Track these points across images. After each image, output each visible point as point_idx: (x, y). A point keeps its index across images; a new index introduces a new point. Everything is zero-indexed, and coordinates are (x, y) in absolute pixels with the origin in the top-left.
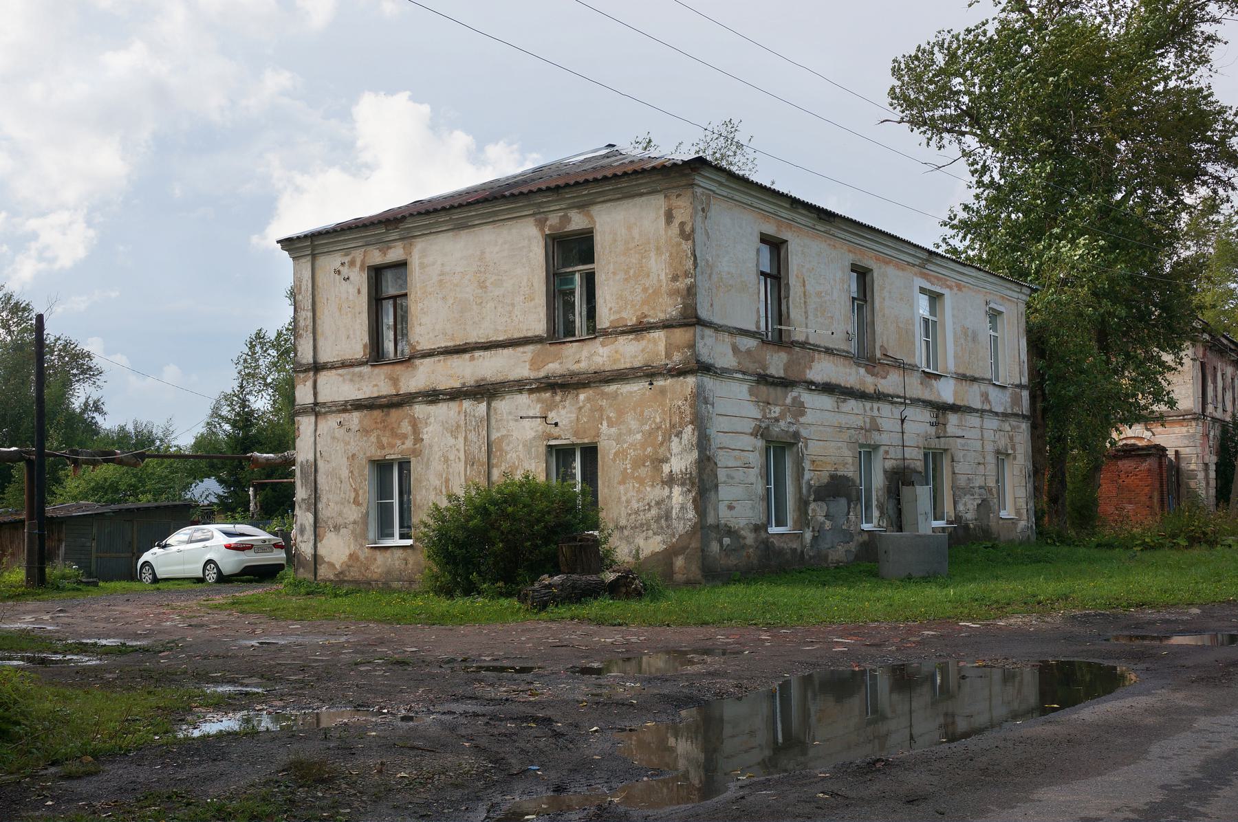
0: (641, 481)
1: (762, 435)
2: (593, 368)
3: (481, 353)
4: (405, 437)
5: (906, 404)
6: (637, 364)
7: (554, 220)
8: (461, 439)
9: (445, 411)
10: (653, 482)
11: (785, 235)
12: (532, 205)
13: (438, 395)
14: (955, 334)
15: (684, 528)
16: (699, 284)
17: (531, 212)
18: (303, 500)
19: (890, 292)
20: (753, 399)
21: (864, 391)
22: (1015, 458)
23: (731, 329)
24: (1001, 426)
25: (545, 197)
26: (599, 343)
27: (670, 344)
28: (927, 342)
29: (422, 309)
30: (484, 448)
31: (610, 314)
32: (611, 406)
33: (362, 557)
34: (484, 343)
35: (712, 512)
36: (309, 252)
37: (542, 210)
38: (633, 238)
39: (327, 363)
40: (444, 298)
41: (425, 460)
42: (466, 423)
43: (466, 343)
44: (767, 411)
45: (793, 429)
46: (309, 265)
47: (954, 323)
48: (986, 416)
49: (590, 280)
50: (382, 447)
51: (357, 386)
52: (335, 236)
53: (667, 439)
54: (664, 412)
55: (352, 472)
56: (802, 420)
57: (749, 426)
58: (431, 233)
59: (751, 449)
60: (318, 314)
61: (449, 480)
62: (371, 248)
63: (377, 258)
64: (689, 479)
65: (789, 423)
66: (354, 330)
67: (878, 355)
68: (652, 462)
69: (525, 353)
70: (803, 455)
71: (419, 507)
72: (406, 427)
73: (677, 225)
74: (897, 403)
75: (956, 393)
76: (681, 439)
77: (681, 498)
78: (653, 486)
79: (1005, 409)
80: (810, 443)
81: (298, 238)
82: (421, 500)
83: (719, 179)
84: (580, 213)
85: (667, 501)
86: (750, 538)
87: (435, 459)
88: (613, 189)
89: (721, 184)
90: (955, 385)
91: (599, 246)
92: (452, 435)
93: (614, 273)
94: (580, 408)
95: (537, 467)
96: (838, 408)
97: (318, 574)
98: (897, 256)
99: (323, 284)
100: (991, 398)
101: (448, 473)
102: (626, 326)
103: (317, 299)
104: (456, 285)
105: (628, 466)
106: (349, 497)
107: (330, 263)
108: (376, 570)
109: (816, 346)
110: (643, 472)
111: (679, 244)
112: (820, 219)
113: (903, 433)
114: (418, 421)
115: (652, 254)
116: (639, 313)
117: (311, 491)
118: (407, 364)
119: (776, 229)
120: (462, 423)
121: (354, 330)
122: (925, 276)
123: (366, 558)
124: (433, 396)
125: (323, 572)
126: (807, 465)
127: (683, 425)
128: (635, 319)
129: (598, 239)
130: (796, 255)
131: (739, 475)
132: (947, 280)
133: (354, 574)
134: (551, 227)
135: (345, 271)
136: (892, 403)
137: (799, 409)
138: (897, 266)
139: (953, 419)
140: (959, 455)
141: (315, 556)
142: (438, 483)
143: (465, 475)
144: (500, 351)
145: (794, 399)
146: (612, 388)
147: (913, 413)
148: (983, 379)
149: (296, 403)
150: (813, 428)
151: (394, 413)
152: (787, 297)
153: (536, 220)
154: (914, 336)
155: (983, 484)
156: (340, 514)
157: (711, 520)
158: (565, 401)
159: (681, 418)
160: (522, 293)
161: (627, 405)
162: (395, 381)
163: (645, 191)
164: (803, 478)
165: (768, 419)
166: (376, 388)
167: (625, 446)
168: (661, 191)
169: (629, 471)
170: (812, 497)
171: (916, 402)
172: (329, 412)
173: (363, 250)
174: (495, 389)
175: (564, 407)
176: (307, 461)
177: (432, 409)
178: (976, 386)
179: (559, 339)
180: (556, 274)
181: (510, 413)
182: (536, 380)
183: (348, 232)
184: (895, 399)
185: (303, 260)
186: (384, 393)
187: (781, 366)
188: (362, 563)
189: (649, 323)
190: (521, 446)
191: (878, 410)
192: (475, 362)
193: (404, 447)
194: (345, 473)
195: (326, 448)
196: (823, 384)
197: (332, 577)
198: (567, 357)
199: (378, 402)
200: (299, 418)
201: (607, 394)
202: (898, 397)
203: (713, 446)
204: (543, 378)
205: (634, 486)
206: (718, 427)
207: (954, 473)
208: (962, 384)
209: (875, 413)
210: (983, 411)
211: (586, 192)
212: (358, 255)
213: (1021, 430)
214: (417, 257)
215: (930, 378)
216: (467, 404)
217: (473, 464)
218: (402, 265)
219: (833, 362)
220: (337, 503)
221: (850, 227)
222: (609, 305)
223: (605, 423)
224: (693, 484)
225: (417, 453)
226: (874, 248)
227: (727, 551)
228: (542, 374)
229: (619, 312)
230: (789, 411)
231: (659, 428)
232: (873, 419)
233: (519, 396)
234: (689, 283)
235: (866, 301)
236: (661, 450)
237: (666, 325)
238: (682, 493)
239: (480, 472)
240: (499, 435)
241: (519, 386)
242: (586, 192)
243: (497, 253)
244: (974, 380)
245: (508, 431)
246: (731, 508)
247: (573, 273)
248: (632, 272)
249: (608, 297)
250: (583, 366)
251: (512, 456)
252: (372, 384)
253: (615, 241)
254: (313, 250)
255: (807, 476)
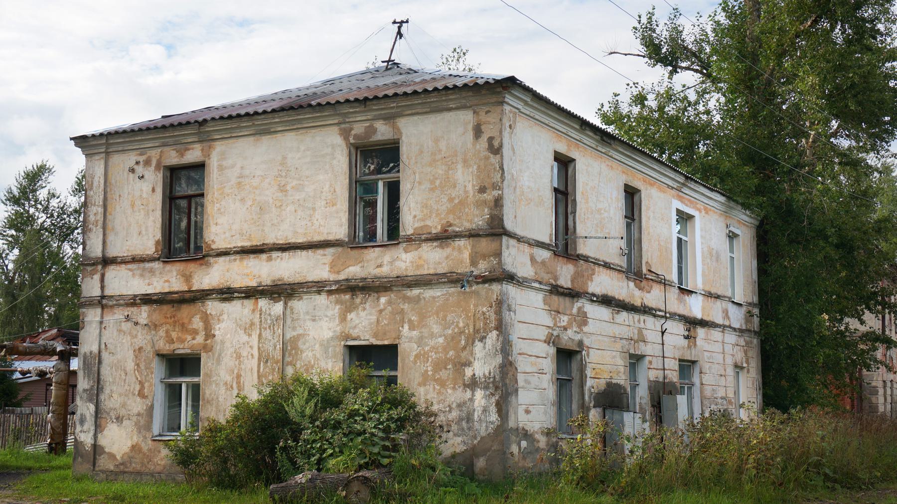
0: (442, 384)
1: (553, 343)
2: (395, 273)
3: (279, 254)
4: (195, 332)
5: (666, 318)
6: (440, 270)
7: (359, 129)
8: (255, 337)
9: (239, 310)
10: (454, 385)
11: (573, 154)
12: (338, 114)
13: (233, 293)
14: (703, 253)
15: (486, 430)
16: (505, 196)
17: (336, 121)
18: (85, 391)
19: (654, 212)
20: (547, 307)
21: (633, 305)
22: (748, 372)
23: (531, 241)
24: (738, 341)
25: (351, 107)
26: (402, 248)
27: (476, 253)
28: (732, 258)
29: (219, 209)
30: (279, 346)
31: (414, 222)
32: (413, 310)
33: (145, 448)
34: (282, 244)
35: (513, 415)
36: (103, 150)
37: (347, 120)
38: (440, 151)
39: (118, 257)
40: (243, 200)
41: (216, 355)
42: (261, 321)
43: (263, 244)
44: (558, 320)
45: (577, 337)
46: (102, 162)
47: (702, 243)
48: (726, 331)
49: (394, 191)
50: (172, 341)
51: (147, 281)
52: (132, 136)
53: (471, 342)
54: (468, 317)
55: (138, 365)
56: (585, 329)
57: (542, 334)
58: (231, 137)
59: (544, 356)
60: (109, 209)
61: (241, 375)
62: (166, 149)
63: (173, 158)
64: (493, 382)
65: (576, 332)
66: (147, 227)
67: (644, 271)
68: (455, 365)
69: (325, 255)
70: (586, 363)
71: (208, 402)
72: (197, 323)
73: (486, 140)
74: (659, 316)
75: (703, 309)
76: (485, 343)
77: (483, 402)
78: (454, 388)
79: (741, 325)
80: (591, 351)
81: (93, 136)
82: (210, 394)
83: (525, 98)
84: (386, 124)
85: (468, 403)
86: (542, 441)
87: (226, 354)
88: (422, 103)
89: (526, 103)
90: (703, 300)
91: (405, 156)
92: (245, 333)
93: (420, 183)
94: (381, 311)
95: (333, 367)
96: (613, 319)
97: (97, 465)
98: (659, 179)
99: (116, 182)
100: (730, 314)
101: (240, 369)
102: (430, 233)
103: (109, 196)
104: (256, 188)
105: (429, 368)
106: (134, 389)
107: (124, 161)
108: (159, 462)
109: (596, 260)
110: (444, 374)
111: (487, 158)
112: (604, 141)
113: (663, 344)
114: (210, 317)
115: (460, 166)
116: (444, 222)
117: (94, 382)
118: (201, 262)
119: (566, 147)
120: (257, 321)
121: (147, 227)
122: (681, 199)
123: (149, 450)
124: (227, 294)
125: (104, 463)
126: (589, 372)
127: (487, 331)
128: (439, 227)
129: (404, 150)
130: (583, 174)
131: (534, 380)
132: (698, 203)
133: (136, 466)
134: (356, 137)
135: (140, 170)
136: (655, 316)
137: (582, 319)
138: (661, 190)
139: (701, 332)
140: (706, 367)
141: (95, 446)
142: (228, 378)
143: (258, 371)
144: (299, 252)
145: (579, 309)
146: (416, 292)
147: (671, 326)
148: (725, 297)
149: (82, 296)
150: (594, 337)
151: (186, 310)
152: (574, 212)
153: (340, 129)
154: (672, 255)
155: (724, 395)
156: (124, 405)
157: (512, 424)
158: (365, 303)
159: (485, 324)
160: (323, 198)
161: (430, 309)
162: (188, 278)
163: (454, 106)
164: (586, 385)
165: (559, 327)
166: (167, 284)
167: (427, 349)
168: (470, 107)
169: (430, 373)
170: (592, 405)
171: (673, 316)
172: (116, 305)
173: (159, 150)
174: (292, 289)
175: (364, 309)
176: (91, 353)
177: (227, 307)
178: (718, 302)
179: (360, 243)
180: (358, 181)
181: (307, 313)
182: (337, 282)
183: (146, 132)
184: (658, 313)
185: (97, 157)
186: (176, 289)
187: (569, 277)
188: (144, 454)
189: (454, 231)
190: (317, 346)
191: (644, 322)
192: (273, 262)
193: (194, 342)
194: (130, 365)
195: (111, 340)
196: (602, 296)
197: (112, 468)
198: (368, 261)
199: (169, 297)
200: (84, 310)
201: (408, 298)
202: (660, 310)
203: (514, 352)
204: (343, 280)
205: (434, 388)
206: (517, 332)
207: (702, 384)
208: (708, 301)
209: (642, 325)
210: (724, 326)
211: (395, 105)
212: (154, 154)
213: (753, 345)
214: (215, 159)
215: (683, 293)
216: (263, 303)
217: (267, 361)
218: (200, 166)
219: (610, 275)
220: (120, 395)
221: (626, 150)
222: (414, 213)
223: (406, 327)
224: (497, 388)
225: (207, 348)
226: (644, 171)
227: (525, 454)
228: (342, 277)
229: (423, 220)
230: (575, 321)
231: (462, 333)
232: (640, 331)
233: (318, 297)
234: (497, 195)
235: (633, 220)
236: (464, 355)
237: (473, 235)
238: (485, 397)
239: (274, 370)
240: (295, 333)
241: (319, 287)
242: (395, 105)
243: (299, 159)
244: (718, 297)
245: (305, 330)
246: (528, 412)
247: (378, 180)
248: (438, 183)
249: (412, 205)
250: (385, 270)
251: (307, 355)
252: (163, 280)
253: (422, 152)
254: (107, 148)
255: (589, 383)
